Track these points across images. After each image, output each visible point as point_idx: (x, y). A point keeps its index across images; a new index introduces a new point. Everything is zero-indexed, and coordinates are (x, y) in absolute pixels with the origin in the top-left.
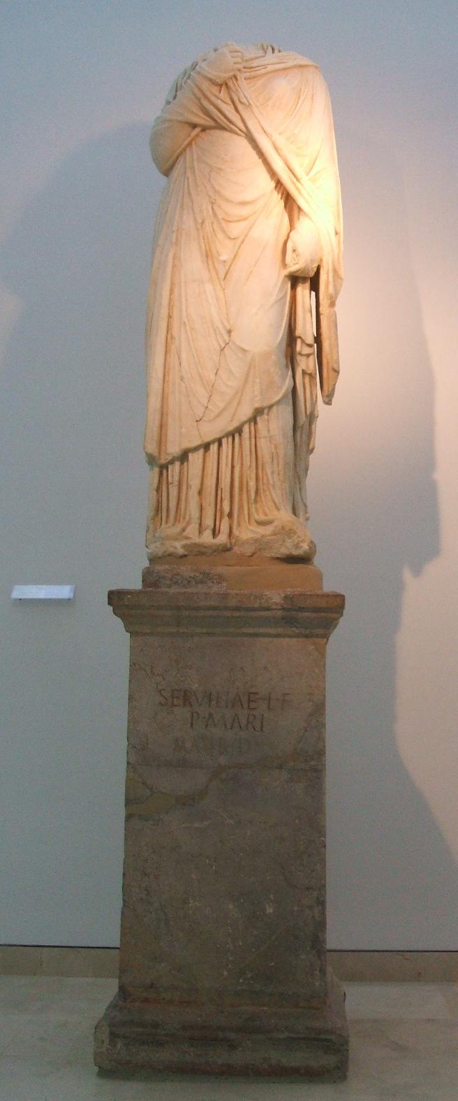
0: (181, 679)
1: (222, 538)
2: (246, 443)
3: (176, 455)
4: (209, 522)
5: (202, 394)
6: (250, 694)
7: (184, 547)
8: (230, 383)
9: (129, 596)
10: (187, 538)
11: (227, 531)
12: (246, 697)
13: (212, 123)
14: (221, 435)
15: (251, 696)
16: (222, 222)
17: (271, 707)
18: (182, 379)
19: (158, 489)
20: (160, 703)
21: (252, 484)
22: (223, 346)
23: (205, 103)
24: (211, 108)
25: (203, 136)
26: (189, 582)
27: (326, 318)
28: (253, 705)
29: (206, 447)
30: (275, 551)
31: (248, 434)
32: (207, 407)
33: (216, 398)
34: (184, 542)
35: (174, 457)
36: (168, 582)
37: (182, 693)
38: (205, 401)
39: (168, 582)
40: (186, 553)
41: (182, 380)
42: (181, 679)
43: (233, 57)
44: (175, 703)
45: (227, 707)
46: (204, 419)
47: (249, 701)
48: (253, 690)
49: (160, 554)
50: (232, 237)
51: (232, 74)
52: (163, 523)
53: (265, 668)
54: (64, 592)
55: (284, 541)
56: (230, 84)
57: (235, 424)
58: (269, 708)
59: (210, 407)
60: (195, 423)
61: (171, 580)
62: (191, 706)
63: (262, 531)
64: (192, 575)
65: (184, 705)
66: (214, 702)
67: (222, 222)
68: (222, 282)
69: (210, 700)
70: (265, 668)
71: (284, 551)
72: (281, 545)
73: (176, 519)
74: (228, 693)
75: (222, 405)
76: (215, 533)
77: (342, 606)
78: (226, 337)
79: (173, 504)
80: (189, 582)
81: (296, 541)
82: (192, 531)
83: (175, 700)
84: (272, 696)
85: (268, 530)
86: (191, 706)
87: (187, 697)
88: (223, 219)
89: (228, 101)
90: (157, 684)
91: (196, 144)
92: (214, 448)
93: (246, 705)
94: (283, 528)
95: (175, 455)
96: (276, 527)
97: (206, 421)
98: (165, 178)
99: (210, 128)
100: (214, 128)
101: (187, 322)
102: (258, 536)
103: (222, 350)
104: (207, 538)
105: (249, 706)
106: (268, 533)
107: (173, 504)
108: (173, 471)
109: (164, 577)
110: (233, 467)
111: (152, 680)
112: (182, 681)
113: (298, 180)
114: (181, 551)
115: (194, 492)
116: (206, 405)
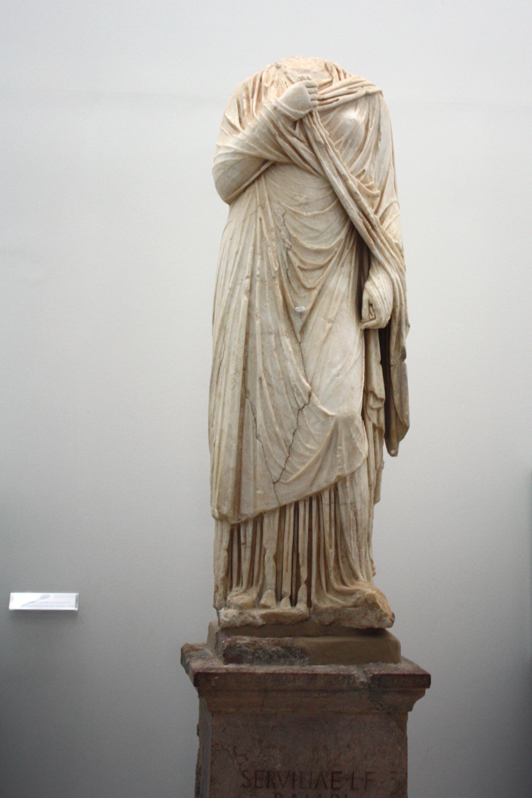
0: (264, 759)
1: (301, 607)
2: (326, 509)
3: (250, 516)
4: (286, 589)
5: (278, 455)
6: (333, 773)
7: (263, 617)
8: (309, 446)
9: (217, 678)
10: (265, 607)
11: (305, 599)
12: (330, 777)
13: (284, 159)
14: (299, 499)
15: (335, 775)
16: (300, 274)
17: (354, 787)
18: (257, 437)
19: (230, 550)
20: (244, 786)
21: (331, 552)
22: (301, 405)
23: (281, 141)
24: (286, 146)
25: (379, 270)
26: (271, 656)
27: (396, 370)
28: (336, 785)
29: (283, 509)
30: (356, 622)
31: (328, 499)
32: (284, 469)
33: (294, 460)
34: (264, 612)
35: (248, 518)
36: (250, 657)
37: (265, 774)
38: (282, 463)
39: (250, 657)
40: (264, 623)
41: (257, 437)
42: (264, 759)
43: (310, 93)
44: (258, 784)
45: (310, 787)
46: (281, 480)
47: (332, 780)
48: (336, 769)
49: (238, 623)
50: (308, 286)
51: (307, 111)
52: (234, 585)
53: (348, 746)
54: (64, 601)
55: (366, 614)
56: (306, 121)
57: (315, 489)
58: (352, 788)
59: (288, 468)
60: (272, 485)
61: (253, 654)
62: (274, 787)
63: (340, 602)
64: (274, 649)
65: (268, 786)
66: (297, 783)
67: (300, 274)
68: (299, 336)
69: (294, 781)
70: (348, 746)
71: (365, 623)
72: (363, 617)
73: (250, 583)
74: (311, 773)
75: (302, 469)
76: (294, 602)
77: (428, 685)
78: (306, 399)
79: (245, 566)
80: (271, 656)
81: (379, 615)
82: (268, 598)
83: (258, 781)
84: (355, 776)
85: (351, 601)
86: (274, 787)
87: (269, 779)
88: (299, 267)
89: (302, 137)
90: (240, 764)
91: (266, 183)
92: (290, 513)
93: (329, 785)
94: (366, 601)
95: (249, 516)
96: (358, 599)
97: (282, 483)
98: (227, 206)
99: (282, 164)
100: (286, 164)
101: (263, 378)
102: (338, 607)
103: (300, 410)
104: (285, 607)
105: (332, 786)
106: (349, 604)
107: (245, 566)
108: (245, 531)
109: (246, 652)
110: (310, 530)
111: (235, 760)
112: (264, 761)
113: (373, 227)
114: (260, 621)
115: (269, 555)
116: (284, 467)
